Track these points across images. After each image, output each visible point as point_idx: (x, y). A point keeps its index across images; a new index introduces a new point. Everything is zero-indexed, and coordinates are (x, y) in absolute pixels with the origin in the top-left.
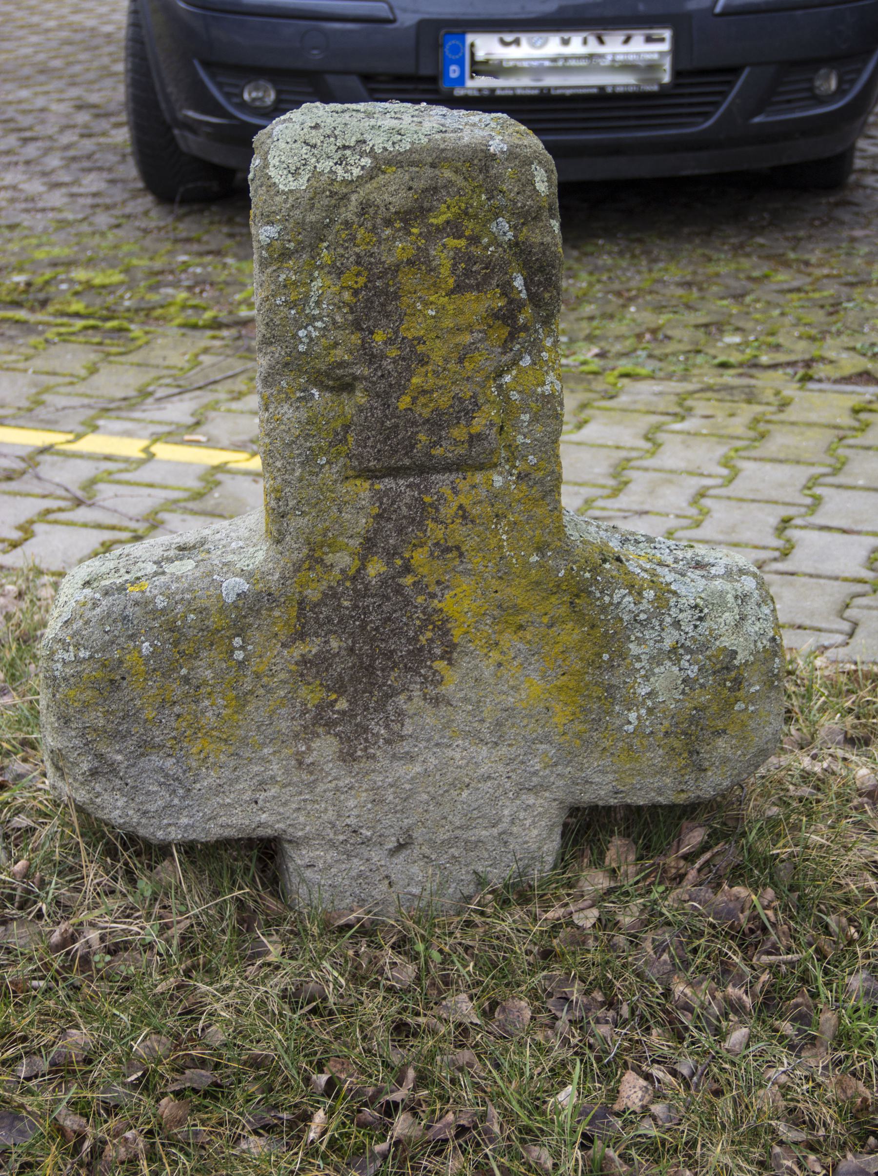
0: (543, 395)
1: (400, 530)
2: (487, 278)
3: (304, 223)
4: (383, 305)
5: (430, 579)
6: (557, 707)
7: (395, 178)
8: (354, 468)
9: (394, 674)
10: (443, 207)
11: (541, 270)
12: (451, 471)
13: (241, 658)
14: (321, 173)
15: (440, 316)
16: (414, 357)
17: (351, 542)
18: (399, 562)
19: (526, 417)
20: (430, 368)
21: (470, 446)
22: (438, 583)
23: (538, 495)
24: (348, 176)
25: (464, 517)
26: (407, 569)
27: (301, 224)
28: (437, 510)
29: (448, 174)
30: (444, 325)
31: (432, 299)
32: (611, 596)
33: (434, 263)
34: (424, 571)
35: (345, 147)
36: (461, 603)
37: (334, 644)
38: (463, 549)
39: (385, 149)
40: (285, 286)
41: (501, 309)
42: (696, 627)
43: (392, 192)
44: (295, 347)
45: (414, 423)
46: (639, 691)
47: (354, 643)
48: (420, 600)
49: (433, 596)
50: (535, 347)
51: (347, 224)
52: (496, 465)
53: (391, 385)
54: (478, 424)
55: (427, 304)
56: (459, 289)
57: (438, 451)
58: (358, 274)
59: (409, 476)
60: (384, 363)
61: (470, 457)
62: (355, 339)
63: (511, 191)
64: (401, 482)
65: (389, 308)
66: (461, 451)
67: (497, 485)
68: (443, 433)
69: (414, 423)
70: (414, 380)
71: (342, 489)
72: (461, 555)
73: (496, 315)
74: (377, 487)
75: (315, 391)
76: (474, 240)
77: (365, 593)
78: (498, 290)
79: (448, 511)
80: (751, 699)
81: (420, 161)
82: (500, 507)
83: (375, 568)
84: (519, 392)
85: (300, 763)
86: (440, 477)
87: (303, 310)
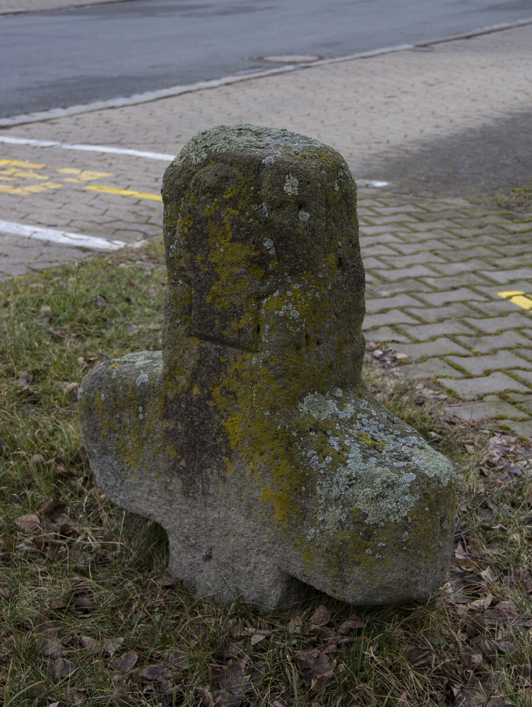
2: (247, 237)
6: (277, 509)
9: (205, 456)
13: (141, 418)
22: (225, 410)
26: (209, 397)
29: (235, 170)
32: (306, 452)
36: (236, 426)
37: (180, 427)
41: (254, 257)
42: (346, 489)
43: (208, 177)
46: (318, 517)
47: (188, 430)
48: (217, 417)
49: (223, 417)
55: (221, 245)
56: (233, 240)
58: (190, 219)
59: (218, 344)
60: (200, 274)
64: (214, 346)
65: (203, 243)
66: (236, 336)
67: (253, 363)
70: (213, 288)
72: (236, 398)
77: (190, 403)
78: (254, 246)
80: (376, 550)
85: (166, 488)
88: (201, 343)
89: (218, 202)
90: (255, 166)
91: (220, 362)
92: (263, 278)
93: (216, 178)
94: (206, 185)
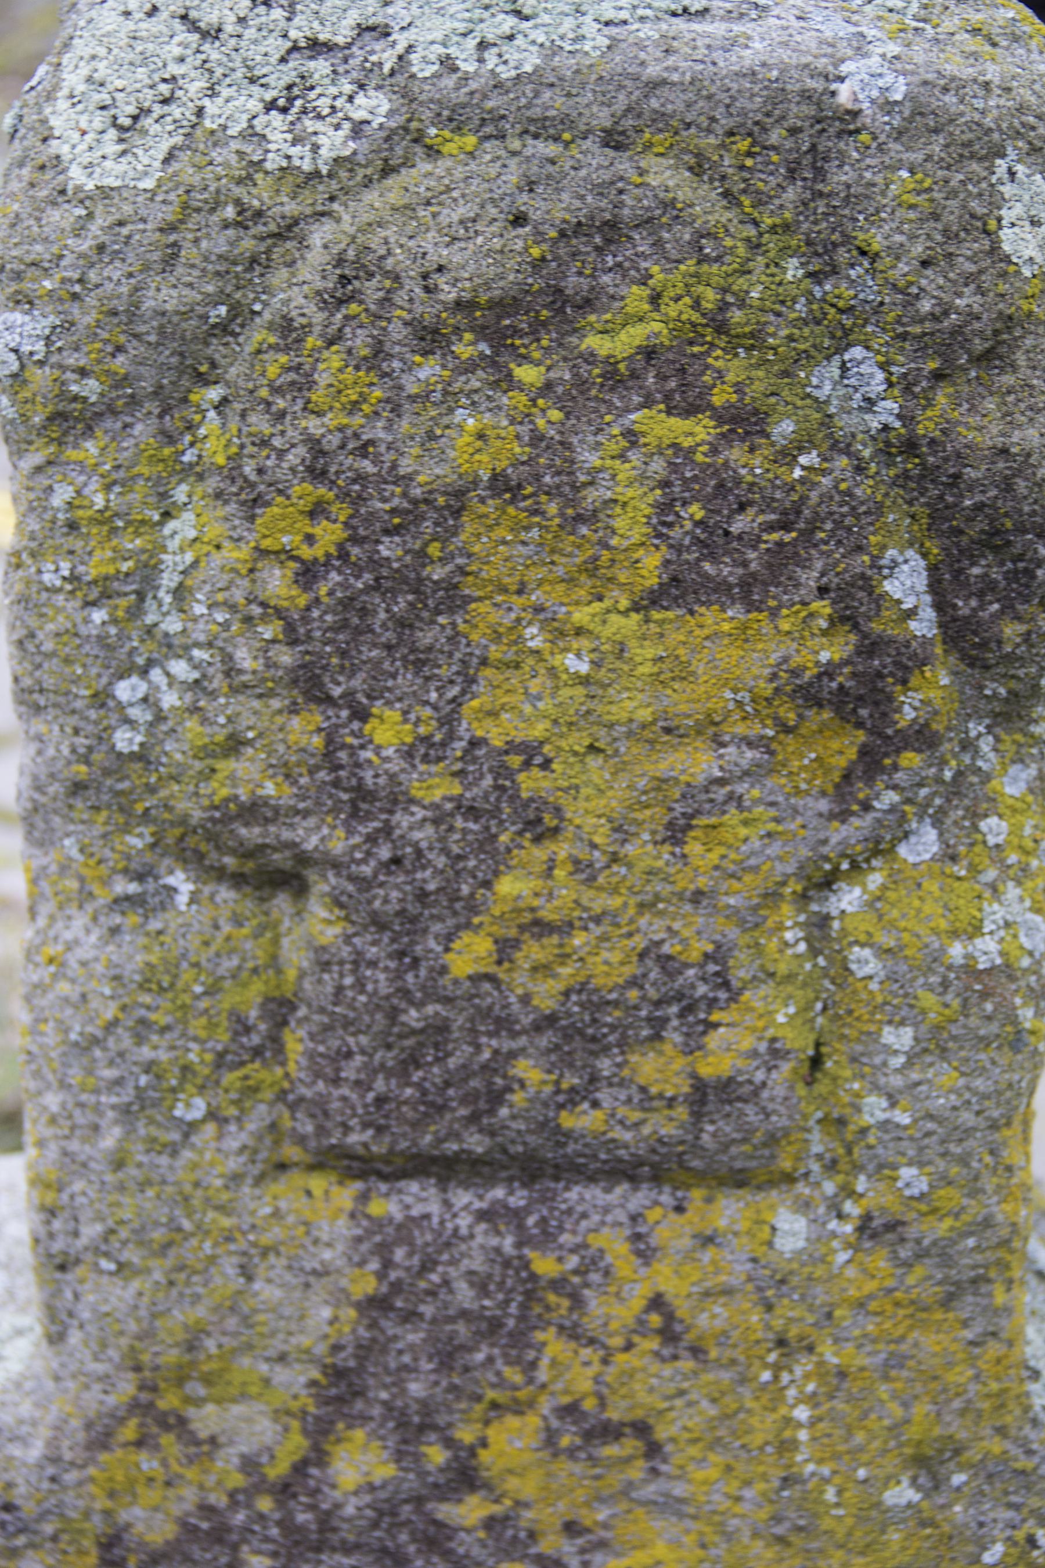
0: (969, 969)
1: (448, 1355)
2: (782, 561)
3: (133, 313)
4: (403, 624)
5: (544, 1517)
7: (470, 176)
8: (301, 1140)
10: (636, 297)
11: (994, 541)
12: (634, 1180)
14: (217, 137)
15: (606, 680)
16: (507, 808)
17: (281, 1375)
18: (437, 1455)
19: (900, 1039)
20: (562, 849)
21: (698, 1116)
22: (571, 1528)
23: (931, 1292)
24: (303, 159)
25: (669, 1334)
26: (465, 1476)
27: (125, 315)
28: (577, 1302)
29: (665, 175)
30: (618, 712)
31: (581, 616)
33: (592, 496)
34: (527, 1487)
35: (316, 47)
38: (662, 1433)
39: (448, 64)
40: (72, 526)
41: (828, 671)
43: (455, 229)
44: (104, 736)
45: (504, 1025)
50: (962, 799)
51: (290, 332)
52: (789, 1179)
53: (422, 896)
54: (726, 1051)
55: (561, 633)
56: (675, 591)
57: (584, 1120)
58: (317, 511)
59: (491, 1182)
60: (402, 820)
61: (696, 1147)
62: (305, 730)
63: (897, 253)
64: (462, 1198)
65: (426, 637)
66: (668, 1125)
68: (605, 1066)
69: (504, 1025)
70: (507, 886)
71: (257, 1204)
72: (653, 1450)
73: (809, 693)
74: (377, 1208)
75: (181, 882)
76: (744, 423)
78: (823, 607)
79: (613, 1311)
81: (566, 121)
82: (791, 1314)
83: (359, 1464)
84: (884, 952)
86: (595, 1194)
87: (136, 611)
88: (364, 1197)
89: (548, 386)
90: (794, 131)
91: (533, 1277)
92: (847, 777)
93: (519, 239)
94: (449, 294)
